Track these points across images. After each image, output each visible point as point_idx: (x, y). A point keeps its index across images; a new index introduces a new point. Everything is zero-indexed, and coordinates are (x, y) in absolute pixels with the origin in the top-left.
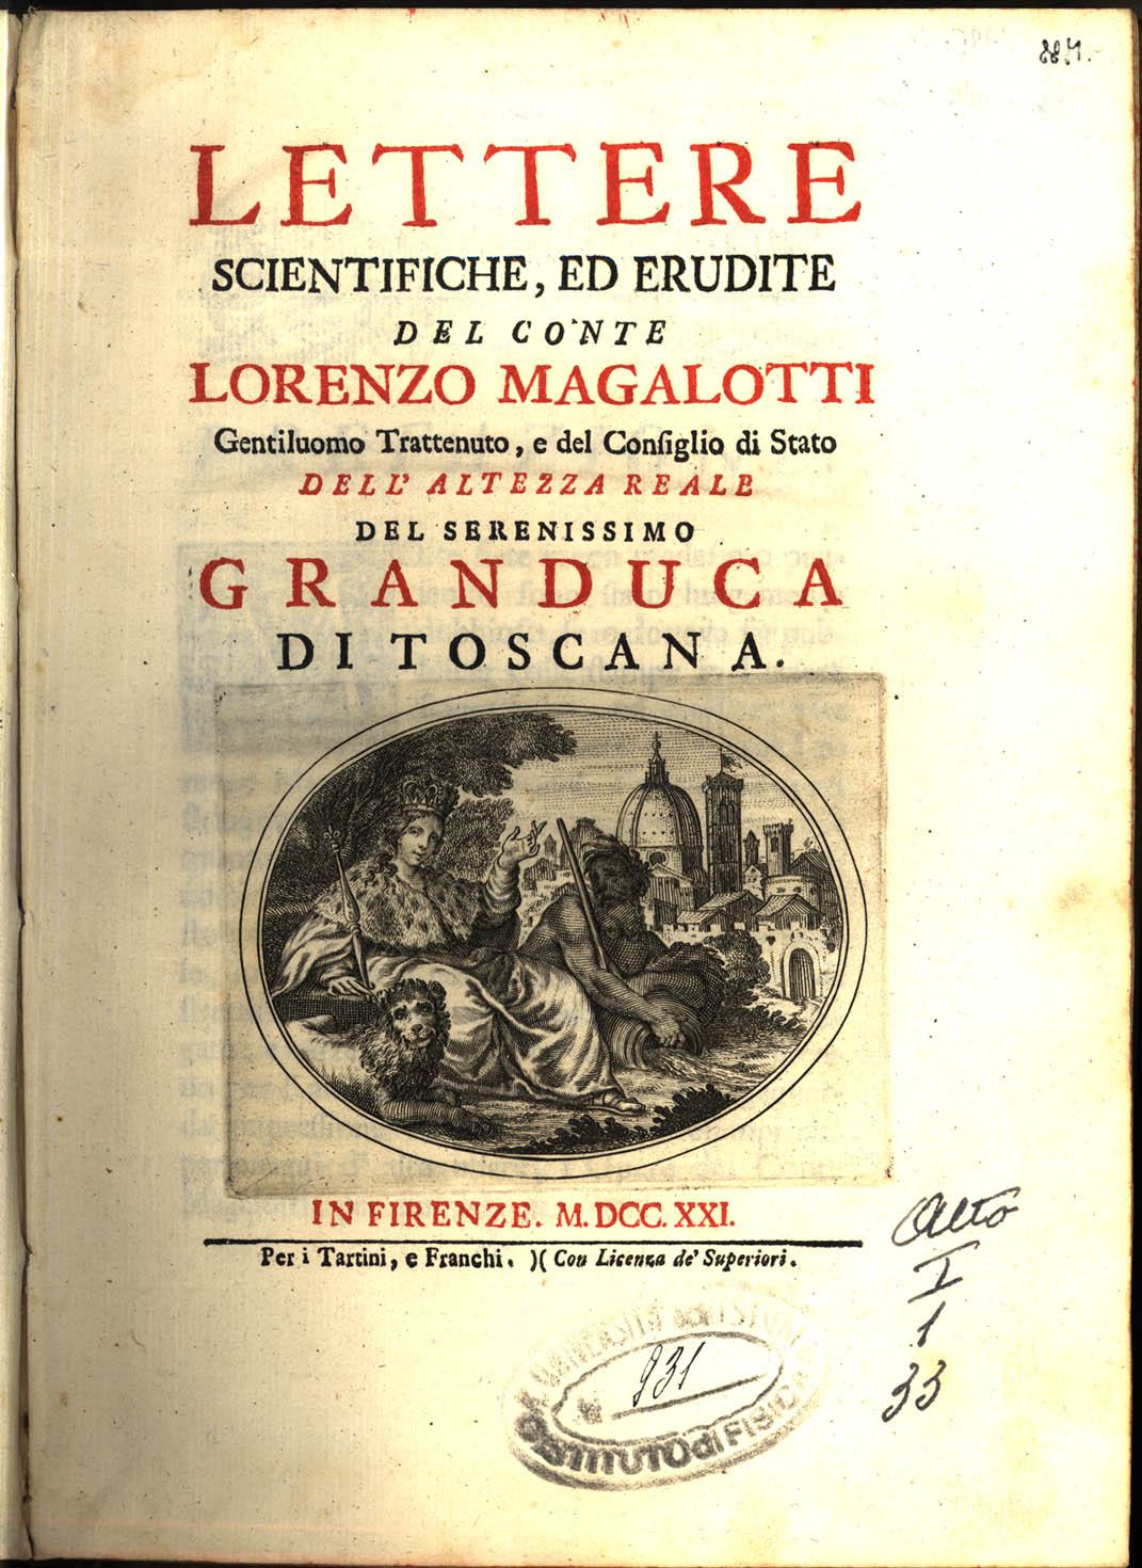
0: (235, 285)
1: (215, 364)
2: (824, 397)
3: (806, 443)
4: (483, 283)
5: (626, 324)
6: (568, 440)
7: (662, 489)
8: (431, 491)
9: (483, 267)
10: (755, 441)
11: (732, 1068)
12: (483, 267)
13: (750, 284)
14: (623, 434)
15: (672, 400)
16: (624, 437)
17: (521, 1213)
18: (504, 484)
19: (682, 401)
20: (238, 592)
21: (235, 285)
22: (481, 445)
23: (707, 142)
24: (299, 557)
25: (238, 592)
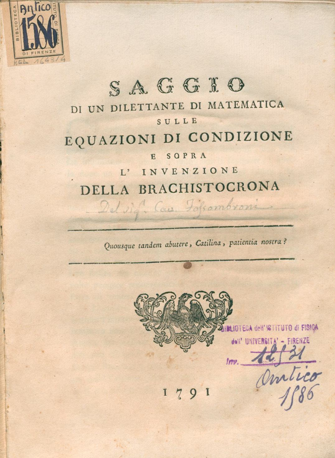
0: (174, 300)
2: (207, 191)
4: (184, 190)
9: (184, 186)
12: (184, 186)
13: (266, 241)
21: (174, 300)
23: (209, 183)
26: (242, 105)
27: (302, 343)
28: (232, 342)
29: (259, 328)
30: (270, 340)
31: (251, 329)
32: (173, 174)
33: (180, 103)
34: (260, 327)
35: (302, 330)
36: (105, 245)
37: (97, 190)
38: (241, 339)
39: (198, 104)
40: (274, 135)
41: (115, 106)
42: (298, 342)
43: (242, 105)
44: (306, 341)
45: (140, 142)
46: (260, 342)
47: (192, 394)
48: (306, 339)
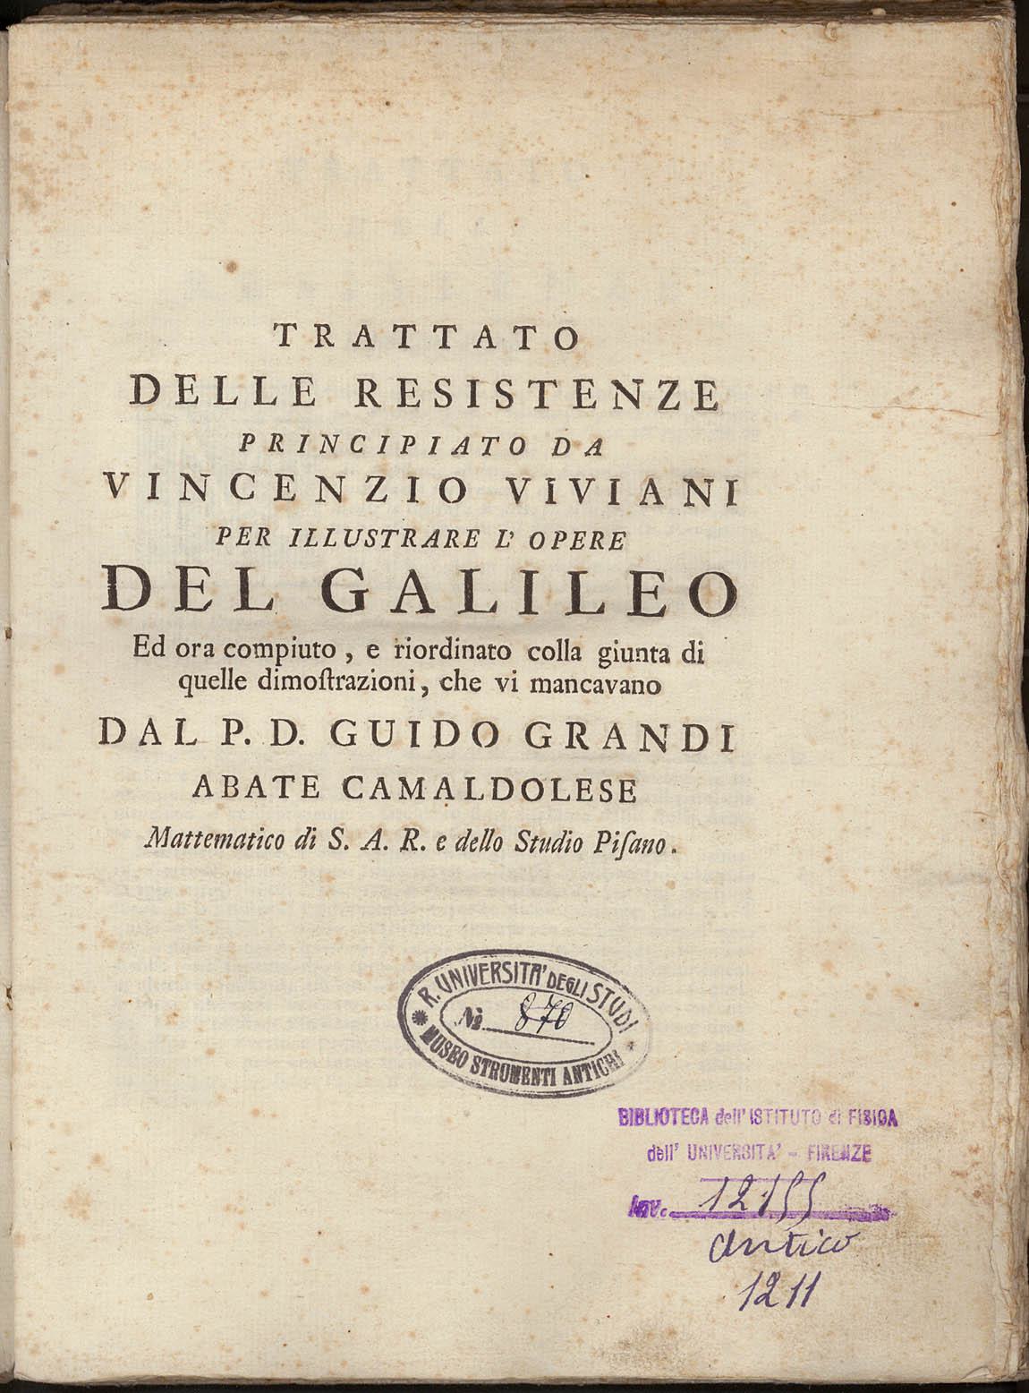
5: (491, 439)
8: (455, 453)
10: (700, 651)
15: (608, 682)
17: (240, 667)
18: (449, 443)
20: (359, 597)
25: (359, 597)
26: (402, 791)
33: (306, 778)
37: (288, 487)
41: (452, 723)
43: (402, 791)
44: (860, 1155)
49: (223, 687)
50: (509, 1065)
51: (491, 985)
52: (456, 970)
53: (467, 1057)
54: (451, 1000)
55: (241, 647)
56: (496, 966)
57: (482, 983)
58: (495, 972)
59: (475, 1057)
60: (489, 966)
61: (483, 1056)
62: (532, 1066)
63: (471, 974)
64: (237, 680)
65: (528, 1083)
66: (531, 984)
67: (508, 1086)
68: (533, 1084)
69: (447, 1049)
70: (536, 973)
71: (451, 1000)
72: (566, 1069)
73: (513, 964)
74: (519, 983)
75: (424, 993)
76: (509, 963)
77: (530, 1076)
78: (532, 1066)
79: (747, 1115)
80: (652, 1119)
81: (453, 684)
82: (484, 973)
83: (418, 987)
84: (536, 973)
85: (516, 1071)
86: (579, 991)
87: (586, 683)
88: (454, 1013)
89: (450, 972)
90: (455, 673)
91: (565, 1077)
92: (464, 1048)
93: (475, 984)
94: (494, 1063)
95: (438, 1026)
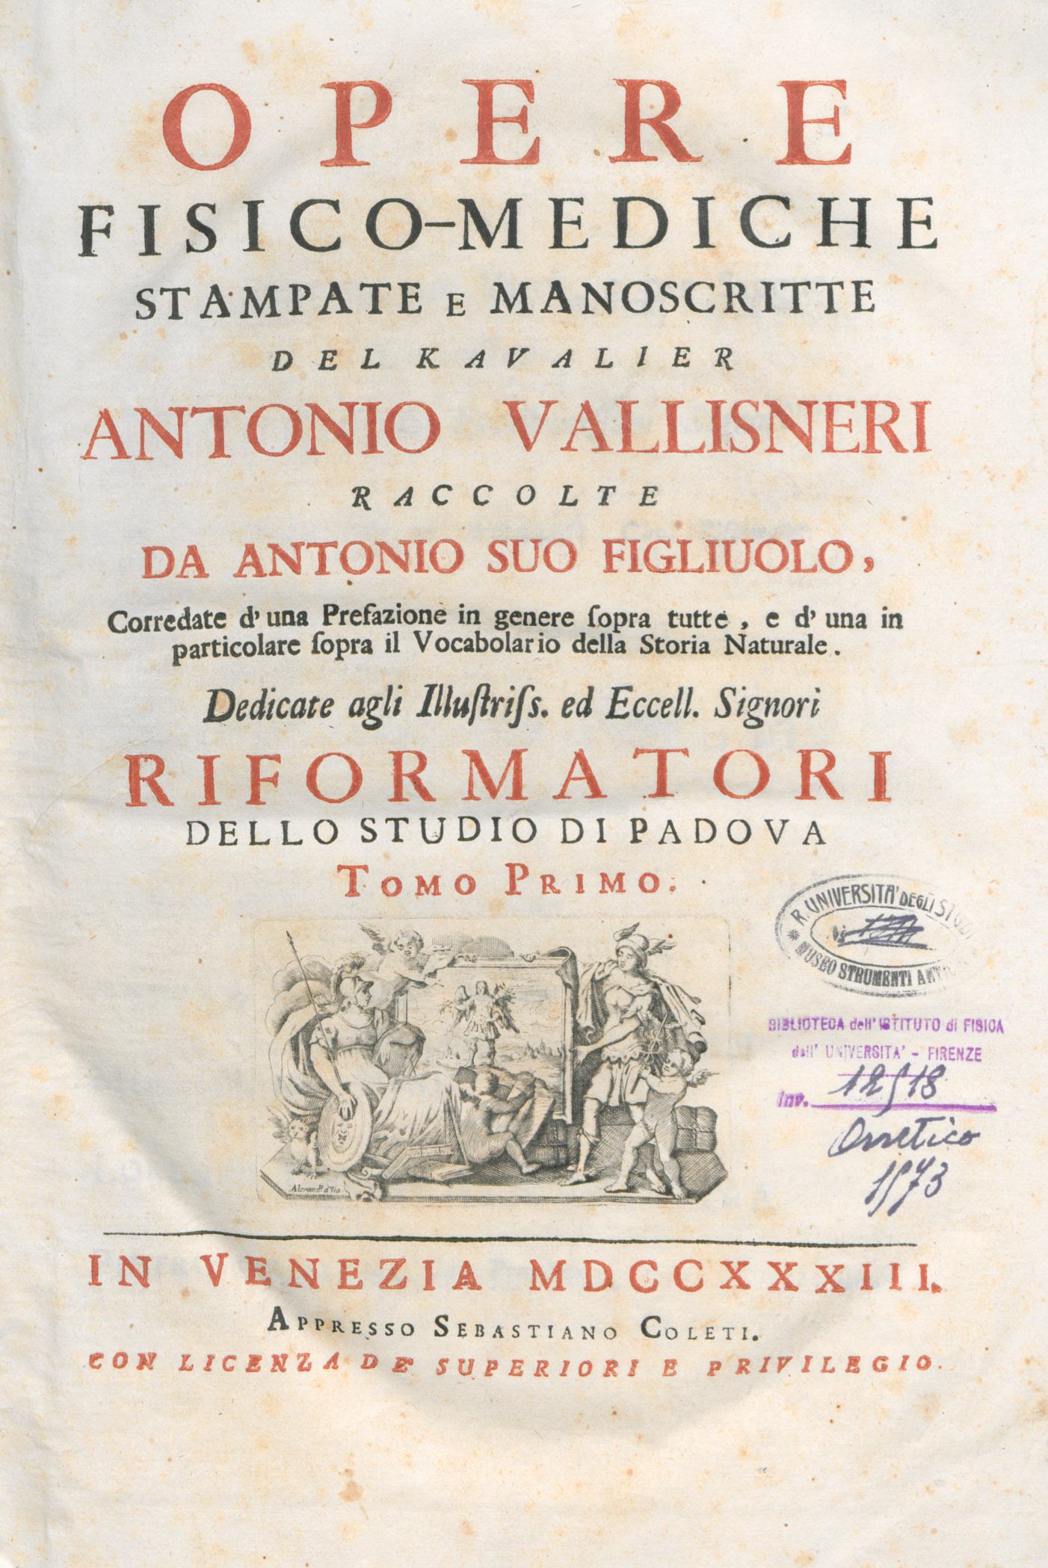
1: (946, 1290)
3: (756, 647)
5: (607, 488)
6: (340, 651)
7: (516, 1371)
11: (576, 1024)
14: (658, 700)
16: (126, 617)
19: (615, 449)
22: (843, 621)
24: (513, 862)
27: (962, 1059)
28: (794, 1051)
29: (861, 1024)
30: (885, 1049)
31: (841, 1024)
32: (340, 1287)
34: (864, 1022)
35: (965, 1030)
36: (460, 556)
38: (816, 1046)
39: (544, 649)
40: (590, 296)
42: (952, 1057)
44: (972, 1056)
45: (772, 444)
46: (862, 1054)
47: (690, 1034)
48: (974, 1052)
49: (602, 651)
50: (871, 971)
51: (853, 905)
52: (823, 894)
53: (835, 965)
54: (819, 918)
55: (133, 619)
56: (856, 888)
57: (845, 904)
58: (855, 893)
59: (842, 965)
60: (850, 889)
61: (849, 964)
62: (891, 970)
63: (835, 896)
64: (818, 644)
65: (888, 985)
66: (886, 902)
67: (871, 988)
68: (893, 985)
69: (817, 960)
70: (890, 894)
71: (819, 918)
72: (919, 972)
73: (870, 886)
74: (877, 902)
75: (796, 914)
76: (867, 885)
77: (890, 978)
78: (891, 970)
79: (877, 1023)
80: (796, 1026)
81: (599, 647)
82: (847, 895)
83: (789, 910)
84: (890, 894)
85: (878, 974)
86: (928, 907)
87: (457, 643)
88: (823, 930)
89: (818, 896)
90: (475, 635)
91: (303, 1029)
92: (832, 958)
93: (839, 904)
94: (859, 969)
95: (810, 941)
